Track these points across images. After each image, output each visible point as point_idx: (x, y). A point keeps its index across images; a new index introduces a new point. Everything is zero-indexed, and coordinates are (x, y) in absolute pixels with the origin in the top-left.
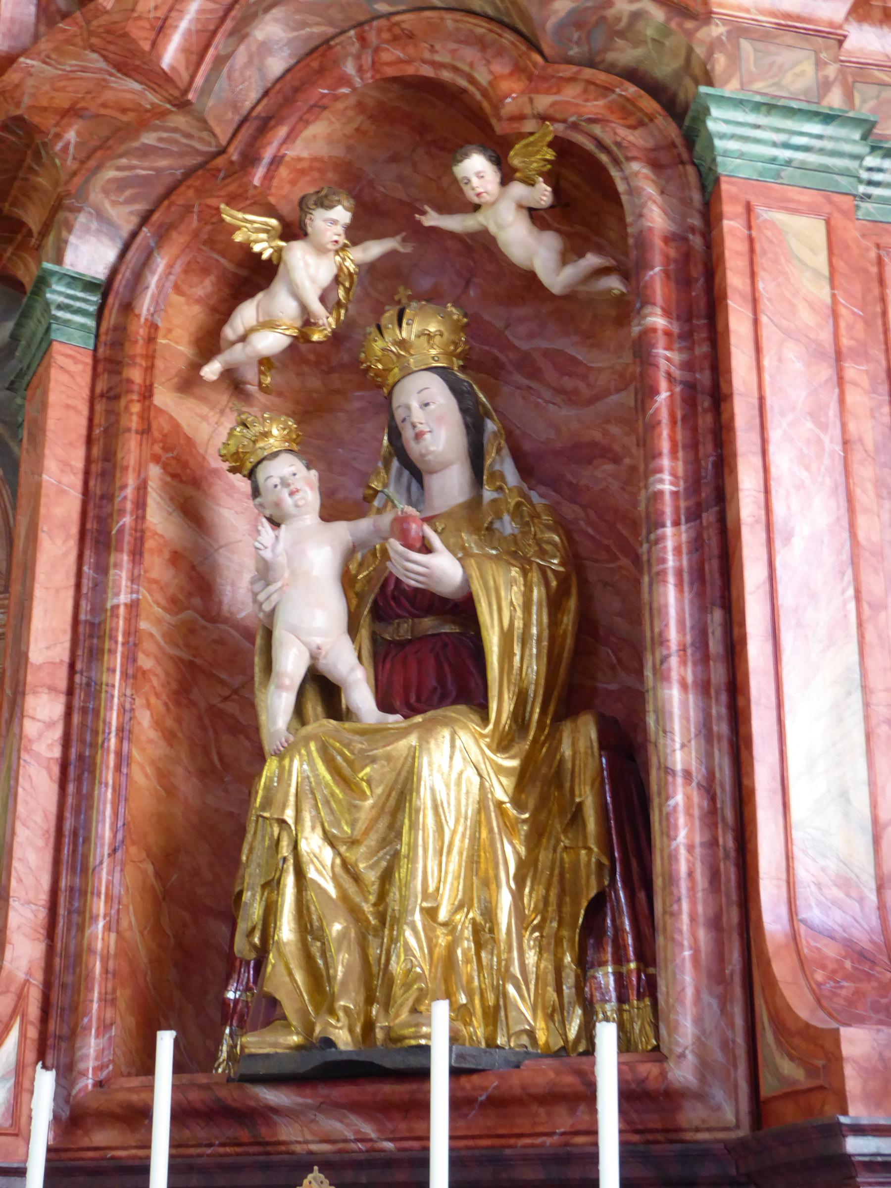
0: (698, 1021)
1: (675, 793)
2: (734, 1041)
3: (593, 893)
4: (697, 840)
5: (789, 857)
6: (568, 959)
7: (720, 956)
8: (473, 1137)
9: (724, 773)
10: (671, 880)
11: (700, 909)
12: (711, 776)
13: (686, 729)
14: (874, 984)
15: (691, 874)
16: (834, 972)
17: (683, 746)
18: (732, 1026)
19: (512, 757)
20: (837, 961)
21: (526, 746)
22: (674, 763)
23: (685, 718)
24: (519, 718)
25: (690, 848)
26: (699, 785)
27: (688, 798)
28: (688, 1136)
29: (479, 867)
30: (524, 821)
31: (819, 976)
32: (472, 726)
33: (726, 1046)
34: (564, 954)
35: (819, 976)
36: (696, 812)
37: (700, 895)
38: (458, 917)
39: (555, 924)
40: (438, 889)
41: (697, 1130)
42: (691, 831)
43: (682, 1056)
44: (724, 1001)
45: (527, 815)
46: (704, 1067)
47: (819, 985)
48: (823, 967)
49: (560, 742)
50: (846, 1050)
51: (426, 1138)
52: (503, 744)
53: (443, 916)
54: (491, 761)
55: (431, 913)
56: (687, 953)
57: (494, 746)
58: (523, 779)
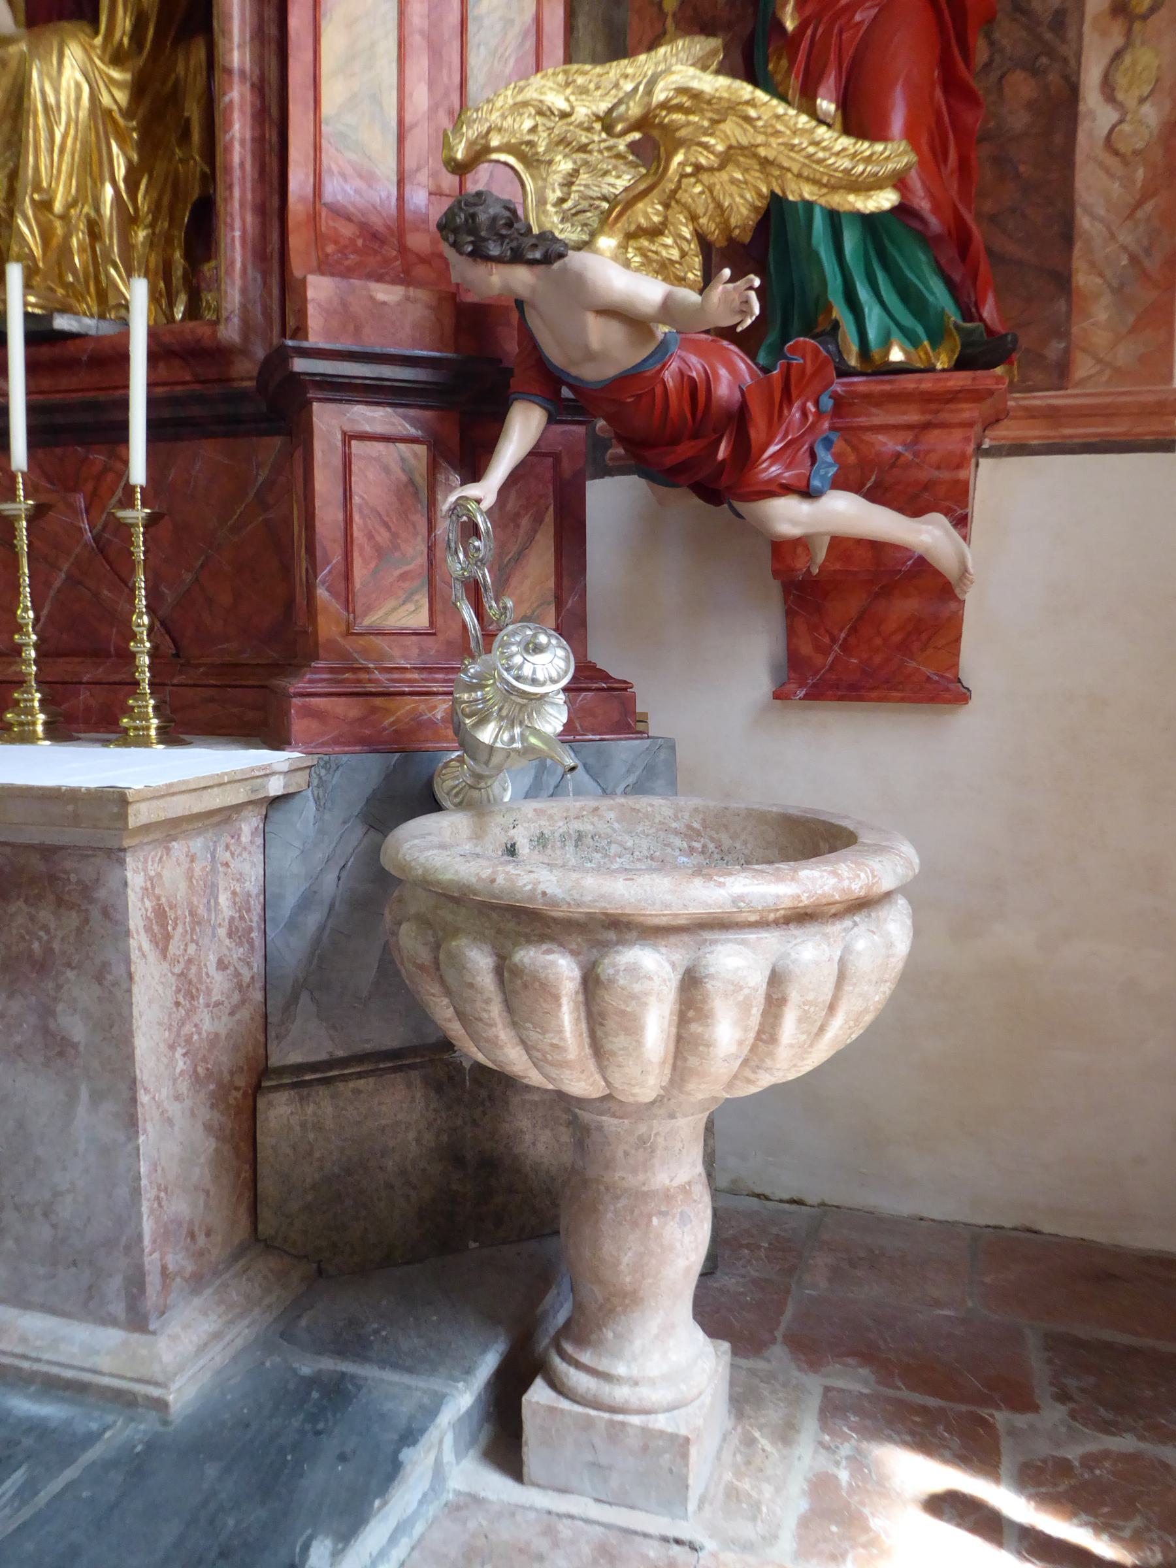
0: (244, 291)
1: (231, 88)
2: (271, 309)
3: (195, 196)
4: (248, 136)
5: (317, 148)
6: (177, 255)
7: (263, 237)
8: (82, 390)
9: (273, 75)
10: (228, 170)
11: (249, 196)
12: (262, 78)
13: (242, 32)
14: (379, 258)
15: (242, 164)
16: (346, 247)
17: (240, 46)
18: (271, 295)
19: (124, 70)
20: (350, 239)
21: (140, 62)
22: (232, 61)
23: (243, 20)
24: (137, 33)
25: (242, 142)
26: (253, 85)
27: (242, 96)
28: (235, 384)
29: (92, 168)
30: (134, 129)
31: (330, 249)
32: (82, 36)
33: (266, 313)
34: (174, 251)
35: (330, 249)
36: (248, 109)
37: (249, 185)
38: (72, 211)
39: (166, 225)
40: (50, 185)
41: (242, 379)
42: (243, 127)
43: (228, 319)
44: (265, 274)
45: (134, 123)
46: (247, 327)
47: (327, 255)
48: (336, 242)
49: (175, 63)
50: (310, 294)
51: (29, 392)
52: (117, 59)
53: (58, 206)
54: (100, 71)
55: (45, 206)
56: (237, 234)
57: (107, 59)
58: (138, 90)
